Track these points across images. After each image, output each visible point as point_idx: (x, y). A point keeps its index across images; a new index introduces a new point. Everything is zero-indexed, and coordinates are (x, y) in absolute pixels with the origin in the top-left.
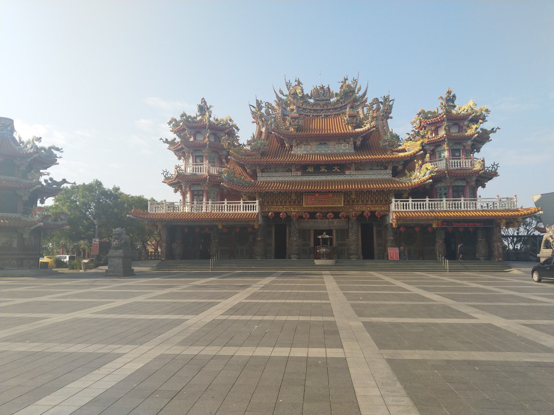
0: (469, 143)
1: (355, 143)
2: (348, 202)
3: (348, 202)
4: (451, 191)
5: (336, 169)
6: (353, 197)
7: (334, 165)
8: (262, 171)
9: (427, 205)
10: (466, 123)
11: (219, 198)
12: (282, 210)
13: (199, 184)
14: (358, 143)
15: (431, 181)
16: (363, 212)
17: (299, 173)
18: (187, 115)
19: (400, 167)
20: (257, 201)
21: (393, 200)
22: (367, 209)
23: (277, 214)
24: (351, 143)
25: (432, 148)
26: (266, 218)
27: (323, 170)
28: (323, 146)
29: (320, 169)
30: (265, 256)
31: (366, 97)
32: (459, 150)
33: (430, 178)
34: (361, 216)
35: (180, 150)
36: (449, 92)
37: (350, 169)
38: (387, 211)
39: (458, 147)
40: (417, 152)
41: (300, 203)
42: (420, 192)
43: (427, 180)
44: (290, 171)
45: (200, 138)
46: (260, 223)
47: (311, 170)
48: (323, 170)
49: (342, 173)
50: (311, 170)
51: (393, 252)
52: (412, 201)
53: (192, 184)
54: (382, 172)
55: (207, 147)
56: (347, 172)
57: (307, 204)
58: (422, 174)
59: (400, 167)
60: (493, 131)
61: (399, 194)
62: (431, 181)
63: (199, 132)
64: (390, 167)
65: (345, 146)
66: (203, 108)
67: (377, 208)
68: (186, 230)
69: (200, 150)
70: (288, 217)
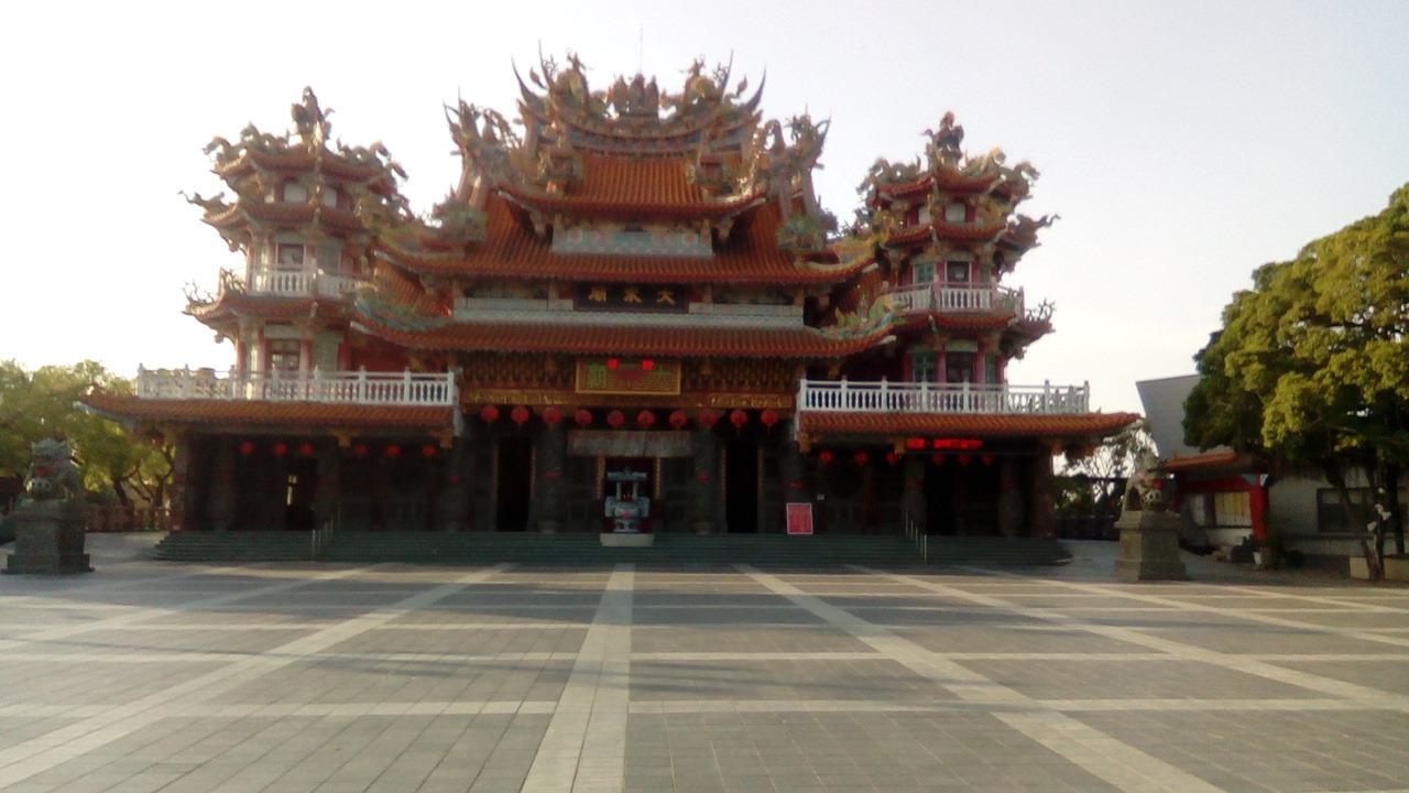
0: (989, 248)
1: (715, 233)
2: (694, 383)
3: (694, 383)
4: (943, 364)
5: (666, 297)
6: (706, 371)
7: (661, 287)
8: (468, 293)
9: (407, 390)
10: (983, 199)
11: (343, 365)
12: (516, 397)
13: (289, 323)
14: (724, 233)
15: (893, 338)
16: (729, 411)
17: (569, 304)
18: (891, 163)
19: (824, 302)
20: (450, 376)
21: (804, 383)
22: (741, 401)
23: (505, 411)
24: (707, 232)
25: (903, 256)
26: (473, 417)
27: (631, 297)
28: (632, 236)
29: (624, 295)
30: (470, 520)
31: (759, 108)
32: (964, 265)
33: (891, 332)
34: (723, 423)
35: (235, 228)
36: (948, 119)
37: (699, 299)
38: (788, 410)
39: (963, 257)
40: (864, 266)
41: (566, 383)
42: (867, 364)
43: (885, 335)
44: (542, 295)
45: (294, 196)
46: (457, 433)
47: (599, 296)
48: (631, 297)
49: (680, 307)
50: (599, 296)
51: (800, 514)
52: (849, 387)
53: (267, 323)
54: (781, 309)
55: (316, 220)
56: (693, 307)
57: (594, 383)
58: (879, 316)
59: (824, 302)
60: (1043, 222)
61: (817, 371)
62: (893, 338)
63: (292, 180)
64: (800, 300)
65: (689, 239)
66: (308, 114)
67: (765, 402)
68: (247, 448)
69: (293, 229)
70: (535, 419)
